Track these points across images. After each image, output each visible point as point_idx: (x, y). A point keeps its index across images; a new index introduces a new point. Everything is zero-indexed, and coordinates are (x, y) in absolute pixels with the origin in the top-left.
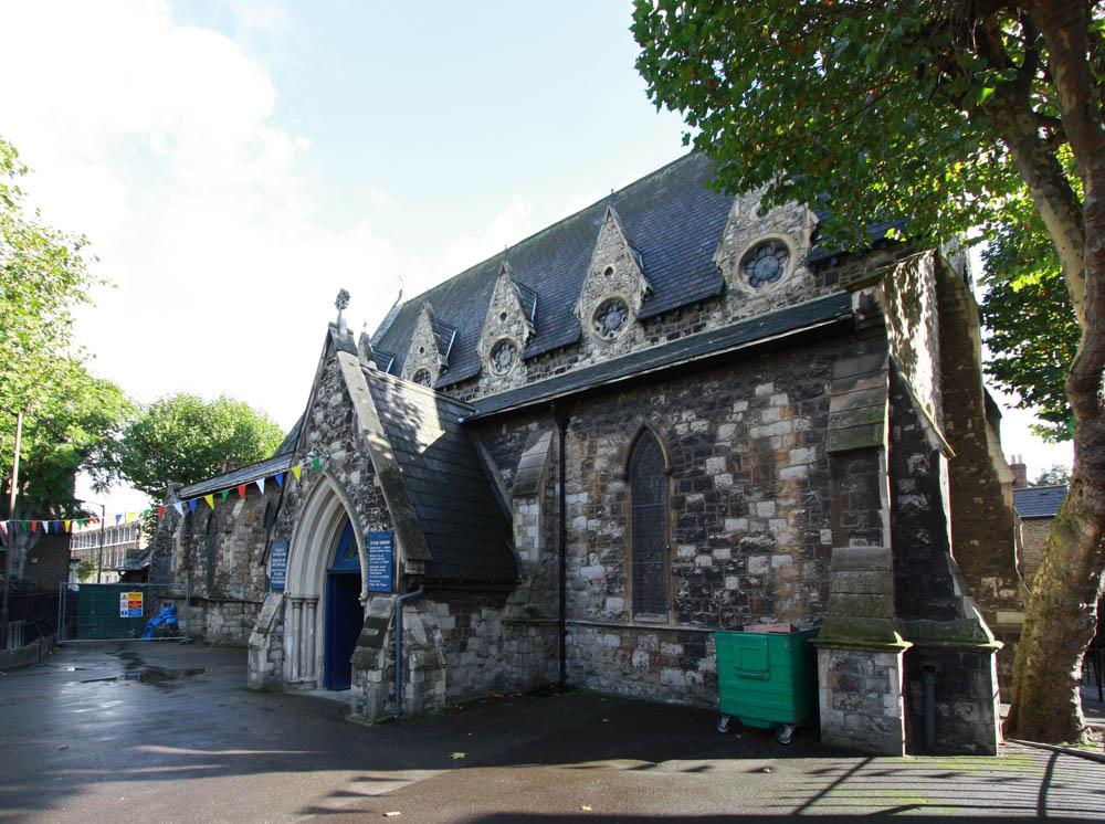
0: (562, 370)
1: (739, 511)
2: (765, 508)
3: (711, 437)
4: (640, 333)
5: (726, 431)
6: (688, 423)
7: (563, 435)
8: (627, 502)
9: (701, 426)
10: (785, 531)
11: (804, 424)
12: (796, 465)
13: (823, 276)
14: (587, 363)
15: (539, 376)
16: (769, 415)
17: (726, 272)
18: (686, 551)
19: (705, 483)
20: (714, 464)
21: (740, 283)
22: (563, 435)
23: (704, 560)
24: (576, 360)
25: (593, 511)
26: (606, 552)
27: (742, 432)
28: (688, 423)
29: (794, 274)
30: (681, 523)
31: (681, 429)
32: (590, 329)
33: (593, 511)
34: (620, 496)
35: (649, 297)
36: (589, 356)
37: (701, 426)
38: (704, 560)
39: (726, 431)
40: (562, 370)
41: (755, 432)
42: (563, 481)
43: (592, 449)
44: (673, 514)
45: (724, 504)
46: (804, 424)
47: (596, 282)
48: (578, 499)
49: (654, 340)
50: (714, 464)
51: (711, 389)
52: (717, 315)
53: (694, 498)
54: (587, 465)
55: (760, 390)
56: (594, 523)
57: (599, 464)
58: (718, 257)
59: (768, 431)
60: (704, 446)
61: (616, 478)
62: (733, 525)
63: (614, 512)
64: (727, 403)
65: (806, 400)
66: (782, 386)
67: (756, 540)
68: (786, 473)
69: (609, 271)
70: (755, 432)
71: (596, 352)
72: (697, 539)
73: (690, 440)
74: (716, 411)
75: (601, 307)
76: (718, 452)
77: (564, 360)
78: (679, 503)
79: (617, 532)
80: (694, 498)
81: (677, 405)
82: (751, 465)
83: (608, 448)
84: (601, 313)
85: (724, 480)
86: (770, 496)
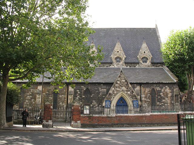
0: (108, 67)
1: (164, 99)
2: (167, 99)
3: (161, 91)
4: (124, 65)
5: (163, 90)
6: (158, 89)
7: (141, 87)
8: (150, 97)
9: (160, 89)
10: (169, 101)
11: (170, 91)
12: (170, 95)
13: (153, 64)
14: (113, 67)
15: (102, 66)
16: (167, 89)
17: (139, 59)
18: (158, 103)
19: (160, 96)
20: (161, 94)
21: (141, 62)
22: (141, 87)
23: (160, 104)
24: (111, 66)
25: (145, 97)
26: (147, 103)
27: (164, 90)
28: (158, 89)
29: (149, 63)
30: (158, 100)
31: (157, 89)
32: (114, 61)
33: (145, 97)
34: (149, 96)
35: (125, 59)
36: (114, 65)
37: (160, 89)
38: (160, 104)
39: (163, 90)
40: (108, 67)
41: (166, 91)
42: (141, 93)
43: (145, 90)
44: (156, 99)
45: (162, 98)
46: (170, 91)
47: (115, 53)
48: (143, 96)
49: (127, 66)
50: (161, 94)
51: (161, 85)
52: (138, 65)
53: (159, 97)
54: (145, 92)
55: (166, 86)
56: (145, 99)
57: (146, 92)
58: (138, 56)
59: (167, 91)
60: (160, 91)
61: (149, 94)
62: (163, 100)
63: (149, 98)
64: (163, 87)
65: (170, 88)
66: (168, 87)
67: (166, 102)
68: (169, 95)
69: (118, 52)
70: (166, 91)
71: (115, 65)
72: (160, 102)
73: (159, 91)
74: (161, 88)
75: (116, 57)
76: (162, 92)
77: (108, 65)
78: (157, 98)
79: (149, 101)
80: (159, 97)
81: (157, 86)
82: (165, 94)
83: (147, 90)
84: (116, 58)
85: (162, 95)
86: (167, 98)
